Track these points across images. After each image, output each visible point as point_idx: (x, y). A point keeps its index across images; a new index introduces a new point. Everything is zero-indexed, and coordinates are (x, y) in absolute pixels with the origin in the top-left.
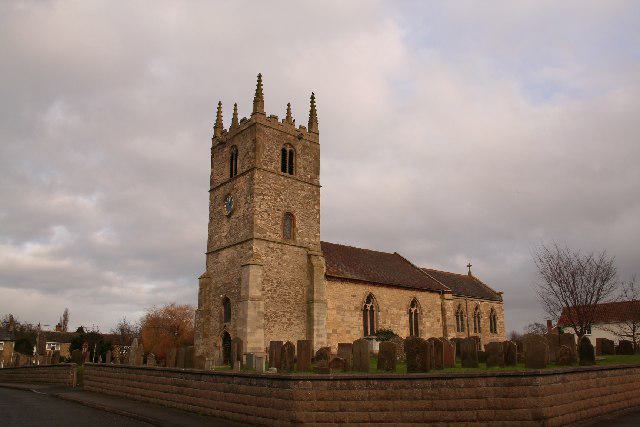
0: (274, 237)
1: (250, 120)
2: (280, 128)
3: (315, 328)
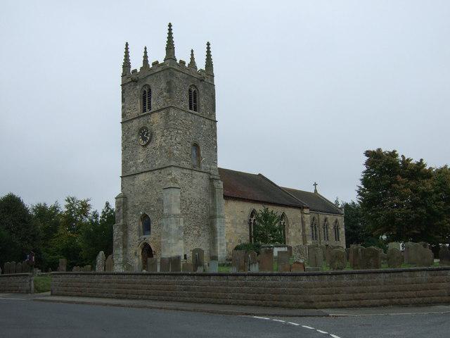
1: (162, 64)
2: (187, 72)
3: (218, 238)
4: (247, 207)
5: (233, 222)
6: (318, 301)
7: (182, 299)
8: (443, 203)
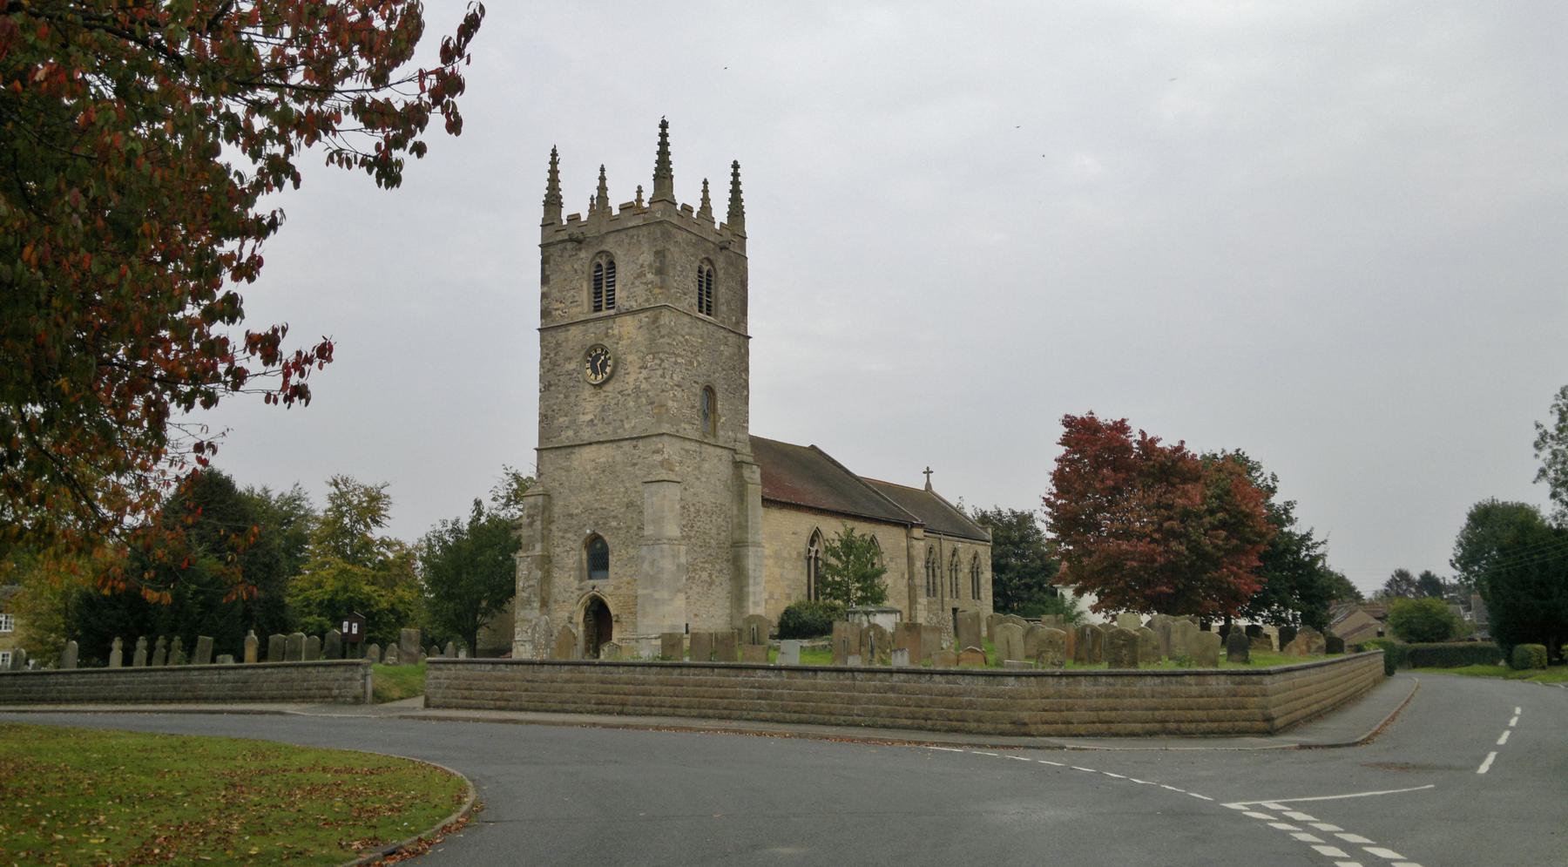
2: (695, 230)
3: (751, 589)
4: (805, 523)
5: (777, 556)
6: (1036, 723)
7: (752, 714)
8: (1223, 534)
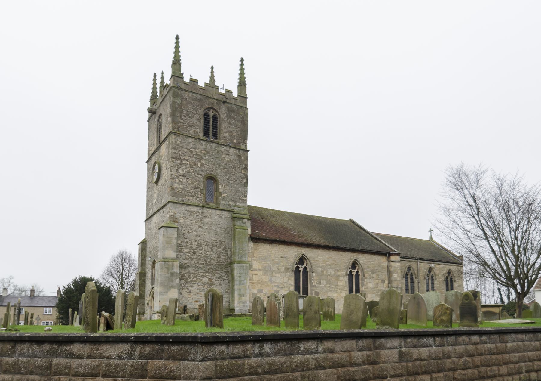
0: (193, 200)
3: (236, 287)
